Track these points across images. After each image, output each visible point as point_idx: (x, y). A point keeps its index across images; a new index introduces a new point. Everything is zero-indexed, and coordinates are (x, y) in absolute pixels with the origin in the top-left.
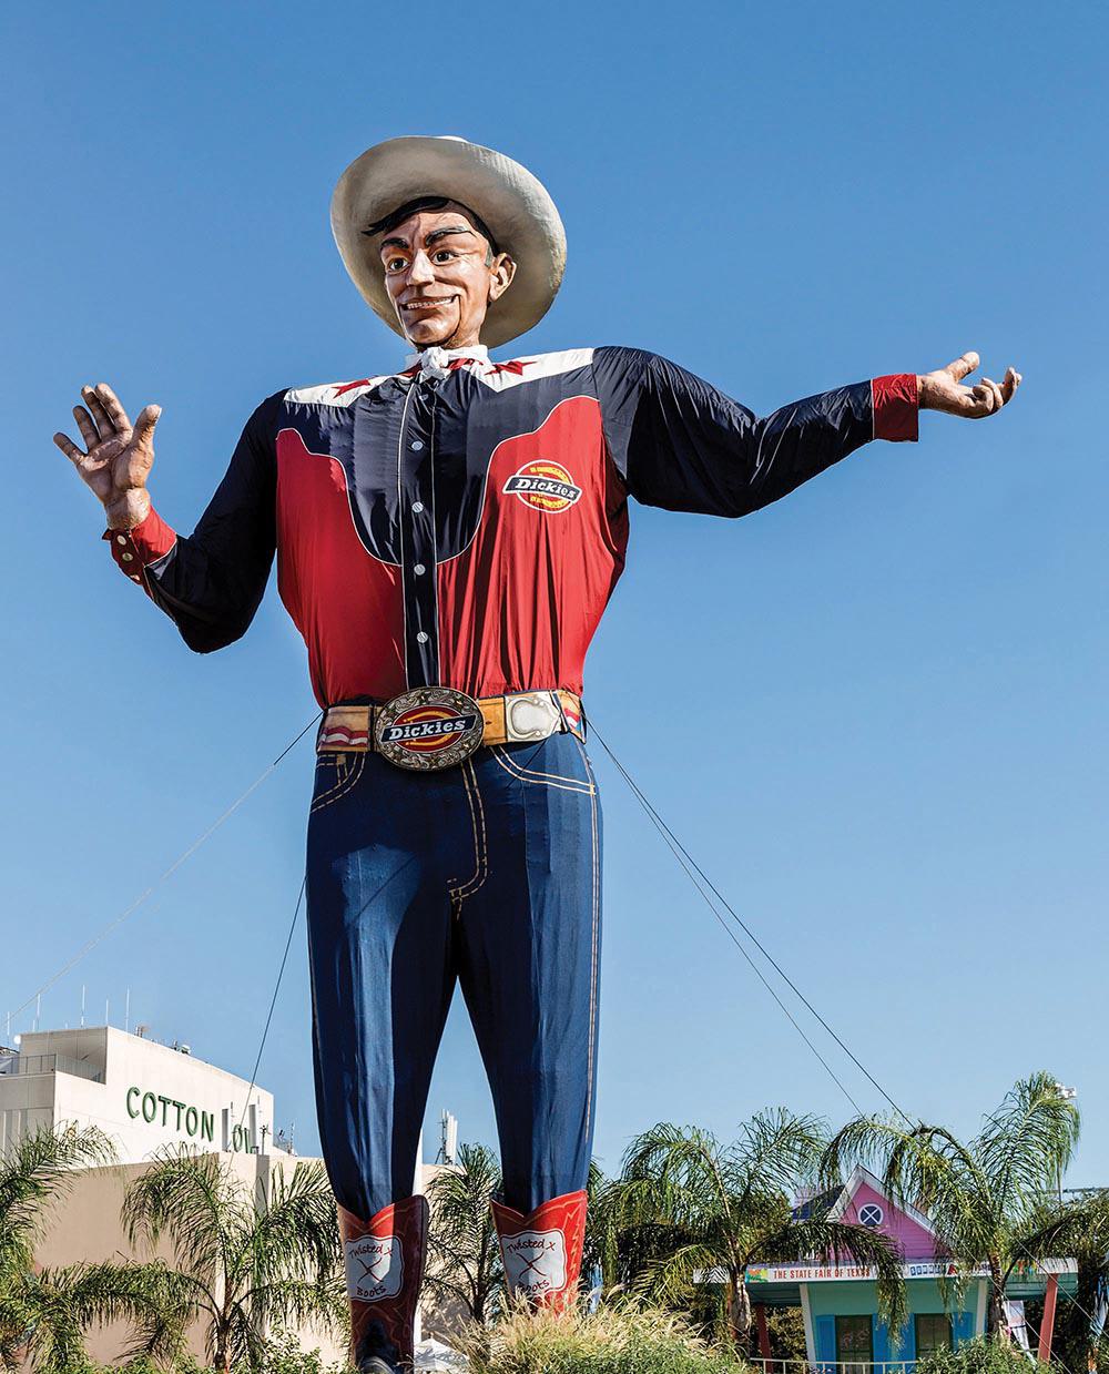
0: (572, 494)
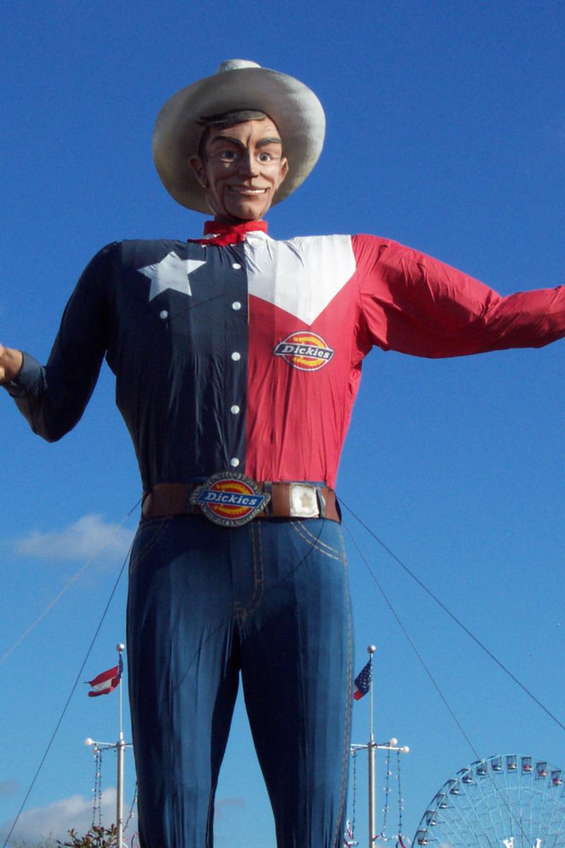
0: (253, 502)
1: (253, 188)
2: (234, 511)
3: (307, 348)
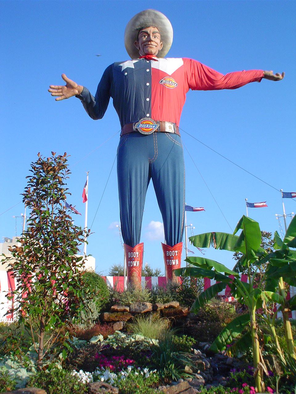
0: (154, 127)
1: (152, 45)
2: (148, 130)
3: (170, 82)
